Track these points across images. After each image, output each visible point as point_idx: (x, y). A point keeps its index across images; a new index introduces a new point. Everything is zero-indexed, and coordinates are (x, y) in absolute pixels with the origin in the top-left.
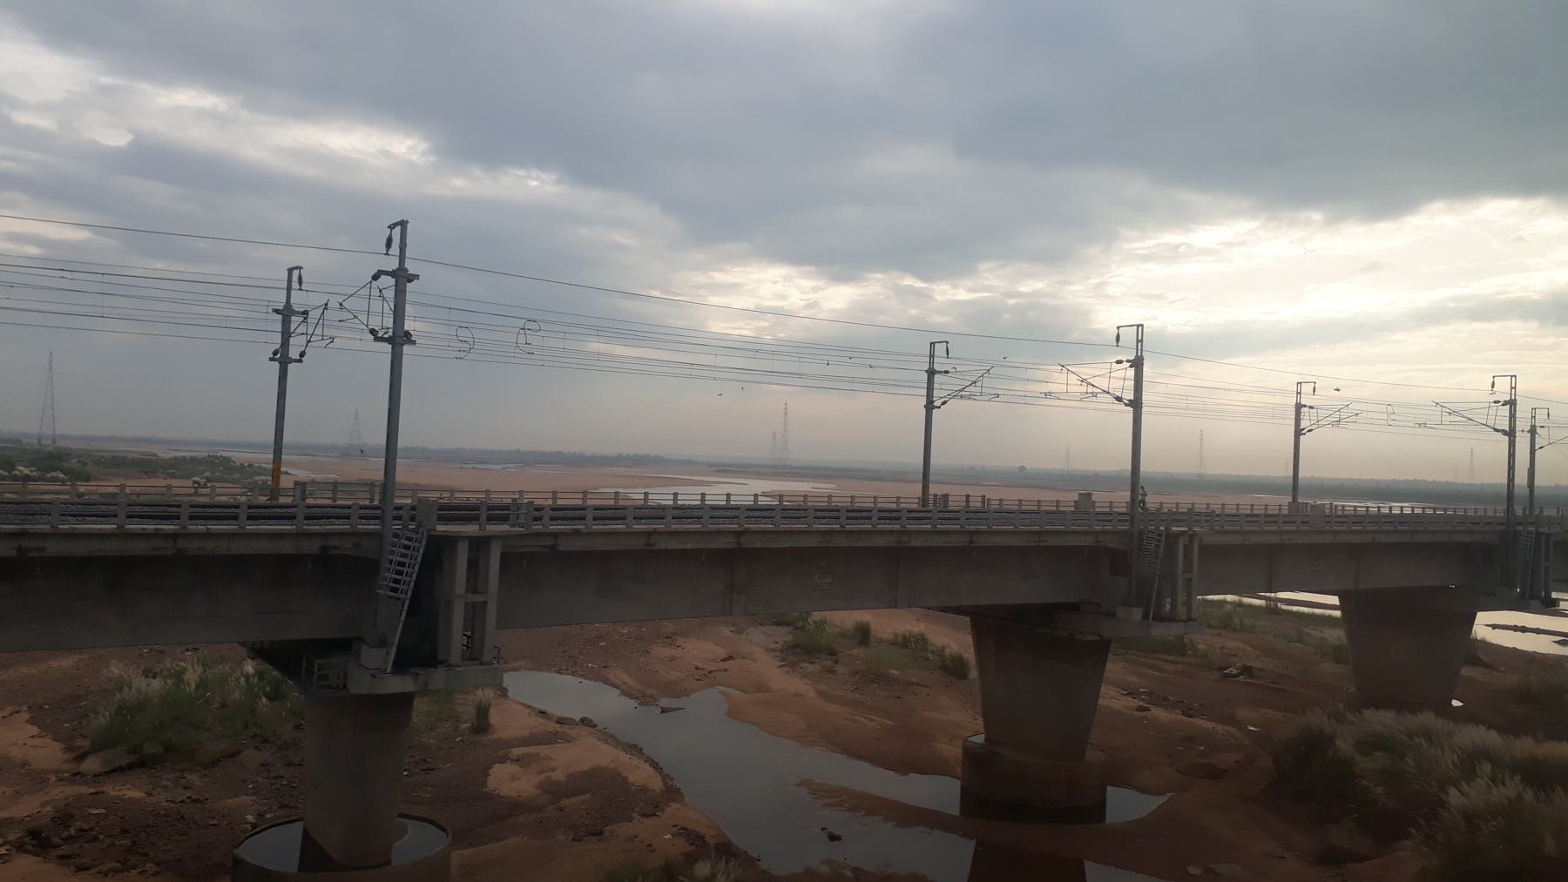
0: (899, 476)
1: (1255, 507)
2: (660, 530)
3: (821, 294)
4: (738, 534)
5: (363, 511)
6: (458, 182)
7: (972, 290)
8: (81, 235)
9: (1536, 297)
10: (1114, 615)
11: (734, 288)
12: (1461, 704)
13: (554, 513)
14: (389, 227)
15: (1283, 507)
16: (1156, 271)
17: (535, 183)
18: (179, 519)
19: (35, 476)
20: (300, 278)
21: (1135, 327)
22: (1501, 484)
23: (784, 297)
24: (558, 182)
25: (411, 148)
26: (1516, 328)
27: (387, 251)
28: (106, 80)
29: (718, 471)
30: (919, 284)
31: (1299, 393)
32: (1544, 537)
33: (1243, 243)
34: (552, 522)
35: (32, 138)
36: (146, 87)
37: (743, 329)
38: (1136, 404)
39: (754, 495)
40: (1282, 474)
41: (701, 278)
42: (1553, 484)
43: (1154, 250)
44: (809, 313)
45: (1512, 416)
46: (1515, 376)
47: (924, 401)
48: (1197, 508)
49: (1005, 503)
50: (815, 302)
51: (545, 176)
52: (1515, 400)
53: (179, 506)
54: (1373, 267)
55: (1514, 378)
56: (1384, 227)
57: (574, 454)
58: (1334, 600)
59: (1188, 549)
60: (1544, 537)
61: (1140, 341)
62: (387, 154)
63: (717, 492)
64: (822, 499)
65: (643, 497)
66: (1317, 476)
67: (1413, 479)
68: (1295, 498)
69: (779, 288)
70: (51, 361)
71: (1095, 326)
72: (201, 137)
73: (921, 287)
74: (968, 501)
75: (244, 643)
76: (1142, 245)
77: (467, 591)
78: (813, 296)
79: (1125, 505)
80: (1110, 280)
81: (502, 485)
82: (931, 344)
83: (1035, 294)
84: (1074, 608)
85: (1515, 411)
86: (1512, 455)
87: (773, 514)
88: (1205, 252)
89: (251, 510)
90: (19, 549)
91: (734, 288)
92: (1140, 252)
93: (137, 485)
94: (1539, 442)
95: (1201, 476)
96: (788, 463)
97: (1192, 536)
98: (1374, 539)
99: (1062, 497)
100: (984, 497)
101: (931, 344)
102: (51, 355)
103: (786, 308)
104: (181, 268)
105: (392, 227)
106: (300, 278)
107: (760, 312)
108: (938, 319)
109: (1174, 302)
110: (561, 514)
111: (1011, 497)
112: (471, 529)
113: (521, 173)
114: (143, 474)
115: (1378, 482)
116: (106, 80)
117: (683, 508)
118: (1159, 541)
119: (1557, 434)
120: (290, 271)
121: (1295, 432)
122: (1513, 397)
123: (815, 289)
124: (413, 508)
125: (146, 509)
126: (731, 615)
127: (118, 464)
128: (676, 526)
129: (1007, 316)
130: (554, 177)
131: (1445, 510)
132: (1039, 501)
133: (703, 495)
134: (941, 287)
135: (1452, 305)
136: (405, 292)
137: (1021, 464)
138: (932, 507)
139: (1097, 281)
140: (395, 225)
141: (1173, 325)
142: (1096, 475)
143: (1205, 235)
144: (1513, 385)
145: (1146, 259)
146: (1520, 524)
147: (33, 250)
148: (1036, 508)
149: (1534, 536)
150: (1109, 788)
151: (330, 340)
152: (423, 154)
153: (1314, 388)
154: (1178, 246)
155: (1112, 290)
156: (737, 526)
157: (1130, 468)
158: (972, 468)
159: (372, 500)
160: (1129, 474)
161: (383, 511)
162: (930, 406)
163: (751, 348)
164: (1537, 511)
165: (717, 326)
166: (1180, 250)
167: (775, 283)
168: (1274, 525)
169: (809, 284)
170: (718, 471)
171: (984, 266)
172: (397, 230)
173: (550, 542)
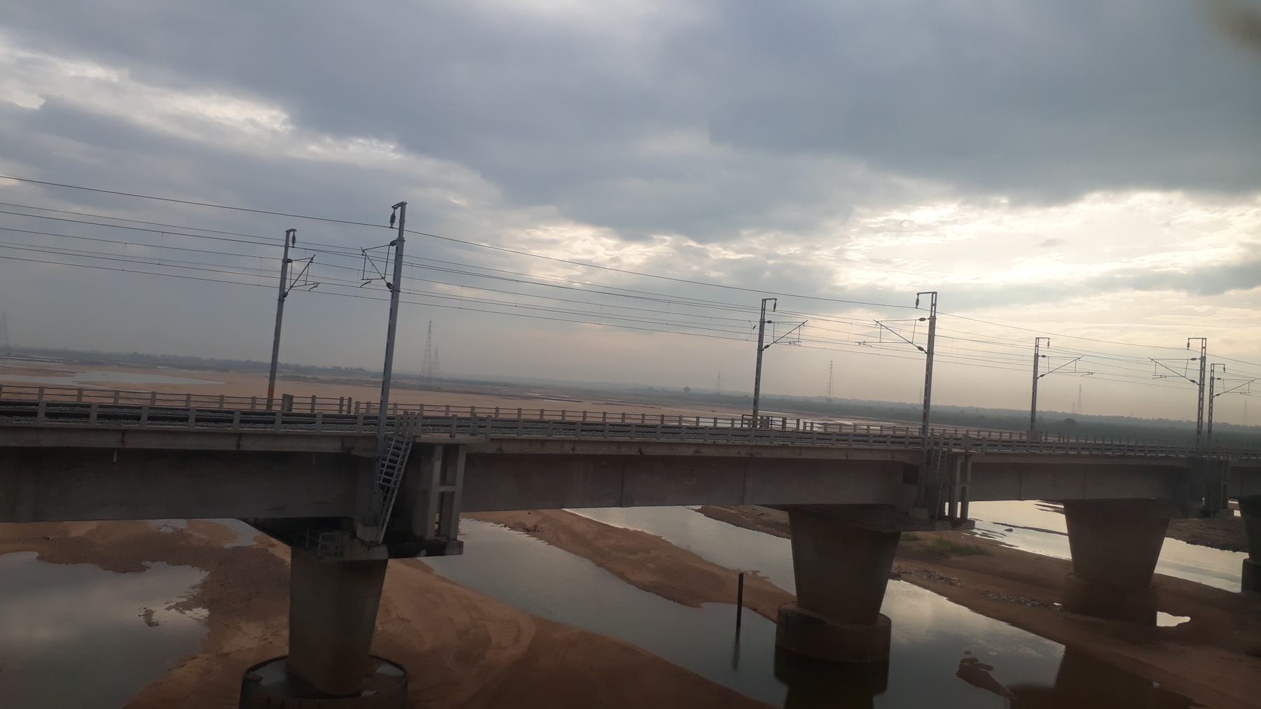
0: (247, 368)
7: (738, 252)
9: (1183, 271)
11: (553, 243)
14: (393, 207)
16: (885, 241)
20: (294, 238)
21: (931, 294)
22: (1189, 422)
23: (592, 252)
24: (394, 151)
26: (1172, 297)
27: (392, 225)
32: (439, 452)
34: (197, 424)
37: (558, 276)
38: (930, 353)
41: (522, 235)
42: (1097, 415)
43: (883, 225)
44: (614, 265)
45: (1203, 369)
46: (1206, 339)
52: (1205, 357)
54: (1051, 243)
55: (1204, 340)
56: (1055, 211)
57: (347, 368)
59: (964, 466)
60: (439, 452)
61: (934, 305)
62: (253, 122)
64: (29, 391)
67: (1157, 418)
69: (587, 245)
72: (103, 104)
75: (246, 519)
76: (874, 221)
78: (616, 253)
79: (918, 430)
82: (763, 300)
84: (334, 524)
85: (1205, 365)
86: (1201, 399)
88: (923, 228)
91: (553, 243)
92: (872, 226)
94: (287, 286)
95: (829, 400)
97: (967, 456)
102: (430, 322)
103: (594, 261)
105: (395, 208)
108: (714, 274)
112: (444, 437)
115: (1167, 421)
117: (859, 435)
119: (1055, 364)
120: (288, 232)
122: (1203, 355)
125: (667, 431)
129: (768, 273)
134: (715, 248)
135: (1119, 276)
136: (402, 255)
137: (684, 387)
138: (758, 429)
139: (839, 248)
140: (398, 205)
143: (924, 214)
145: (876, 231)
148: (601, 420)
150: (1158, 612)
151: (313, 286)
152: (284, 123)
155: (851, 255)
156: (515, 435)
158: (651, 389)
159: (341, 411)
161: (380, 421)
162: (760, 350)
166: (904, 224)
169: (611, 242)
170: (284, 376)
171: (745, 232)
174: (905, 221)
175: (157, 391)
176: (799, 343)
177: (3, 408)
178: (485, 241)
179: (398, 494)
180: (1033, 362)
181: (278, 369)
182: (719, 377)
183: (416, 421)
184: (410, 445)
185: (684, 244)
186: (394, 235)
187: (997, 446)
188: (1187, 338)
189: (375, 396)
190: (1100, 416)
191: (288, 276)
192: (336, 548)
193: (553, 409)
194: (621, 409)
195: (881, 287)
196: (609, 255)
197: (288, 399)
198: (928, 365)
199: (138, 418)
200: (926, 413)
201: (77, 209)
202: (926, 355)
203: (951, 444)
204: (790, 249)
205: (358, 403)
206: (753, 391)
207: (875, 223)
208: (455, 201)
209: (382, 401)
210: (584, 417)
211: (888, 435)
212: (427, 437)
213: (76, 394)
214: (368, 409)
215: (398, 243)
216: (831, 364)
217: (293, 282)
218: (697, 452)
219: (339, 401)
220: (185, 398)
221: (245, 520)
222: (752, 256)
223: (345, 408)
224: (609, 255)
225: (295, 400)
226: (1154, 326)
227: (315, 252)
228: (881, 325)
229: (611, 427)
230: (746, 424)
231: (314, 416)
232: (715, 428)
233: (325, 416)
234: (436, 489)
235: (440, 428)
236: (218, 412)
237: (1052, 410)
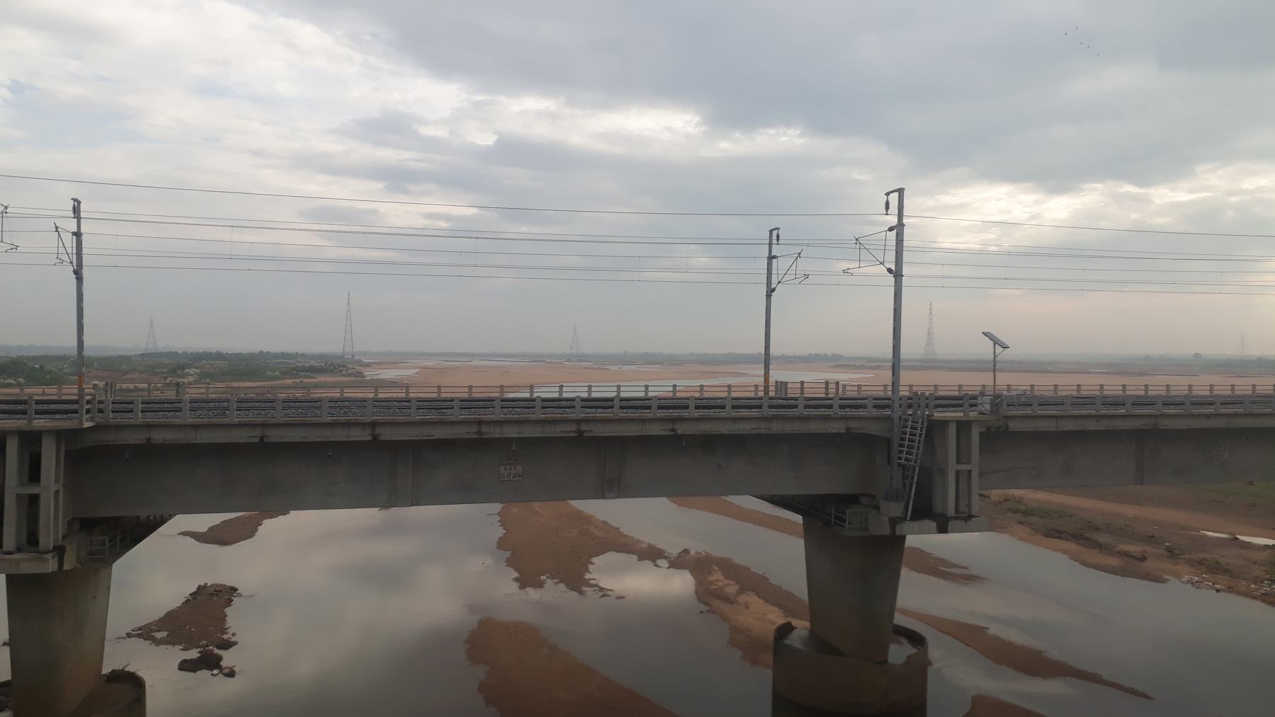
0: (748, 359)
5: (841, 401)
6: (724, 145)
7: (1191, 191)
8: (473, 211)
15: (830, 386)
20: (778, 236)
24: (800, 136)
27: (887, 211)
29: (837, 366)
32: (12, 448)
35: (433, 145)
37: (971, 242)
41: (930, 202)
42: (727, 352)
48: (793, 392)
53: (132, 403)
60: (952, 430)
62: (669, 129)
64: (952, 388)
72: (542, 131)
74: (802, 388)
75: (762, 496)
77: (958, 462)
81: (1179, 384)
84: (853, 499)
87: (365, 403)
89: (545, 403)
91: (961, 207)
94: (774, 280)
98: (262, 438)
99: (1128, 381)
102: (349, 294)
106: (778, 236)
108: (1159, 221)
112: (959, 415)
113: (772, 131)
124: (910, 398)
129: (1230, 213)
132: (1056, 386)
147: (444, 224)
152: (697, 125)
157: (76, 345)
158: (692, 354)
162: (769, 296)
163: (977, 258)
164: (840, 389)
165: (946, 242)
168: (1028, 408)
169: (1031, 198)
170: (837, 366)
171: (1199, 169)
172: (894, 198)
177: (4, 407)
179: (919, 472)
180: (766, 271)
182: (152, 326)
183: (927, 401)
184: (925, 424)
185: (1120, 191)
186: (893, 220)
187: (961, 406)
189: (887, 377)
190: (261, 352)
191: (774, 271)
192: (861, 523)
193: (1067, 384)
194: (1251, 381)
197: (782, 386)
201: (524, 229)
203: (931, 405)
205: (844, 386)
206: (74, 343)
208: (861, 178)
209: (893, 382)
212: (938, 415)
213: (753, 390)
215: (899, 228)
216: (931, 308)
217: (781, 277)
218: (479, 433)
219: (436, 388)
221: (762, 498)
222: (1210, 194)
224: (1026, 213)
225: (789, 385)
227: (802, 248)
228: (860, 244)
229: (734, 401)
231: (534, 400)
232: (376, 400)
233: (544, 400)
234: (952, 466)
236: (755, 399)
237: (732, 352)
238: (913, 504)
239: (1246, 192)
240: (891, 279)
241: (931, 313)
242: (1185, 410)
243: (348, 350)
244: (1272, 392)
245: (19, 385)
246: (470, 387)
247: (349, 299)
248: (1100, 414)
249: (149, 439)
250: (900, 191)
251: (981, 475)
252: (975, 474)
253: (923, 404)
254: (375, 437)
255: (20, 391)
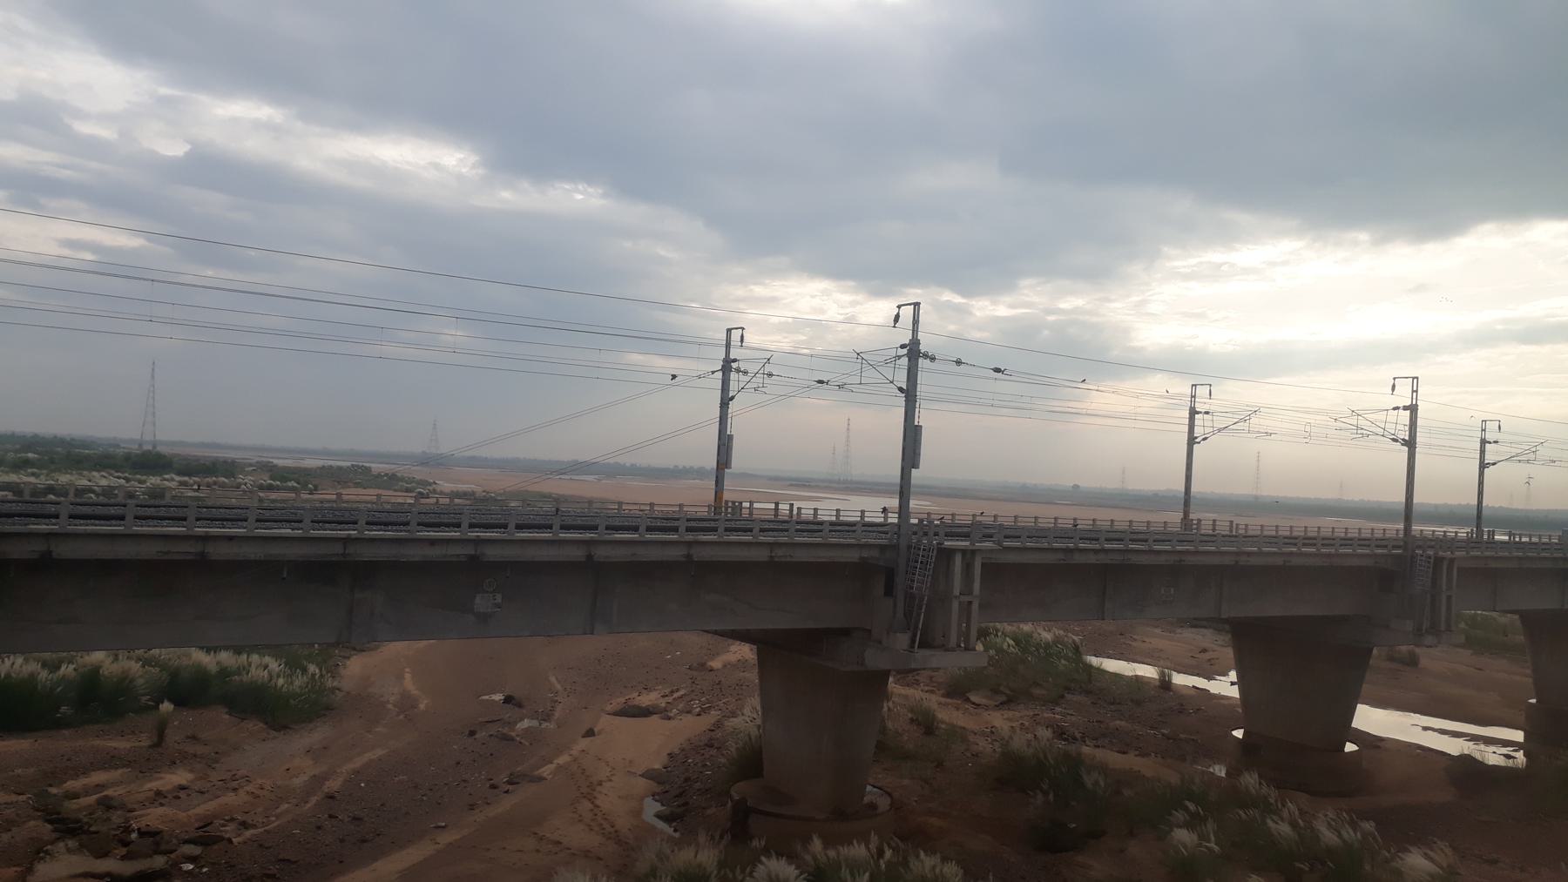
1: (1350, 531)
2: (353, 537)
3: (858, 307)
4: (1237, 554)
6: (506, 195)
7: (1012, 306)
10: (880, 642)
12: (1357, 748)
13: (1343, 542)
15: (1240, 527)
17: (580, 197)
18: (58, 518)
19: (278, 485)
23: (822, 311)
25: (461, 160)
27: (895, 324)
28: (164, 91)
29: (791, 485)
30: (958, 299)
31: (1484, 430)
32: (958, 559)
33: (1285, 263)
35: (92, 147)
36: (203, 98)
38: (1411, 443)
39: (708, 506)
40: (1397, 500)
41: (740, 292)
43: (1195, 269)
46: (1417, 378)
47: (717, 396)
49: (1060, 521)
50: (853, 315)
51: (590, 190)
52: (1417, 405)
54: (1420, 288)
57: (684, 467)
58: (744, 652)
59: (968, 568)
60: (958, 559)
61: (916, 322)
63: (827, 507)
65: (748, 506)
66: (1366, 499)
68: (1186, 514)
70: (153, 370)
71: (1136, 344)
72: (256, 147)
73: (959, 303)
76: (1184, 263)
80: (1150, 298)
82: (1193, 385)
83: (1075, 310)
84: (845, 632)
90: (1285, 561)
91: (773, 300)
93: (367, 495)
95: (1256, 497)
96: (849, 479)
100: (1231, 522)
101: (1193, 385)
104: (231, 276)
107: (798, 325)
108: (977, 335)
109: (1216, 320)
110: (850, 528)
111: (1121, 518)
112: (964, 544)
113: (567, 187)
114: (336, 483)
116: (164, 91)
118: (1429, 562)
121: (1189, 438)
122: (1414, 403)
123: (854, 304)
126: (592, 634)
127: (338, 476)
128: (949, 543)
129: (1046, 332)
130: (600, 191)
131: (1530, 536)
133: (816, 510)
134: (980, 303)
135: (1499, 327)
137: (1072, 485)
139: (1139, 298)
141: (1214, 344)
142: (1156, 495)
143: (1247, 255)
144: (1415, 389)
145: (1187, 277)
146: (1419, 547)
147: (89, 256)
149: (1432, 561)
153: (742, 337)
154: (1221, 265)
159: (1231, 531)
160: (1404, 505)
164: (795, 512)
166: (1222, 268)
167: (813, 297)
169: (847, 298)
170: (791, 485)
171: (1025, 282)
173: (470, 550)
174: (1225, 263)
175: (1169, 521)
176: (763, 389)
178: (692, 301)
181: (912, 489)
182: (1341, 487)
187: (787, 530)
188: (1392, 378)
190: (1468, 504)
193: (1066, 515)
194: (1213, 516)
195: (1189, 346)
196: (842, 314)
198: (1409, 459)
199: (595, 528)
200: (1479, 516)
202: (1406, 449)
203: (252, 519)
204: (1074, 302)
206: (1182, 489)
207: (1184, 267)
208: (663, 253)
210: (1360, 533)
211: (1300, 536)
214: (1246, 530)
220: (1344, 530)
223: (1234, 530)
224: (842, 314)
226: (1537, 390)
228: (863, 359)
230: (1514, 538)
235: (869, 534)
238: (921, 635)
239: (1062, 311)
240: (902, 400)
241: (848, 429)
242: (1217, 547)
243: (148, 437)
244: (706, 514)
245: (293, 489)
246: (863, 512)
247: (153, 370)
248: (309, 535)
249: (1237, 562)
250: (917, 305)
251: (981, 606)
252: (975, 606)
253: (931, 533)
254: (590, 557)
255: (450, 501)
